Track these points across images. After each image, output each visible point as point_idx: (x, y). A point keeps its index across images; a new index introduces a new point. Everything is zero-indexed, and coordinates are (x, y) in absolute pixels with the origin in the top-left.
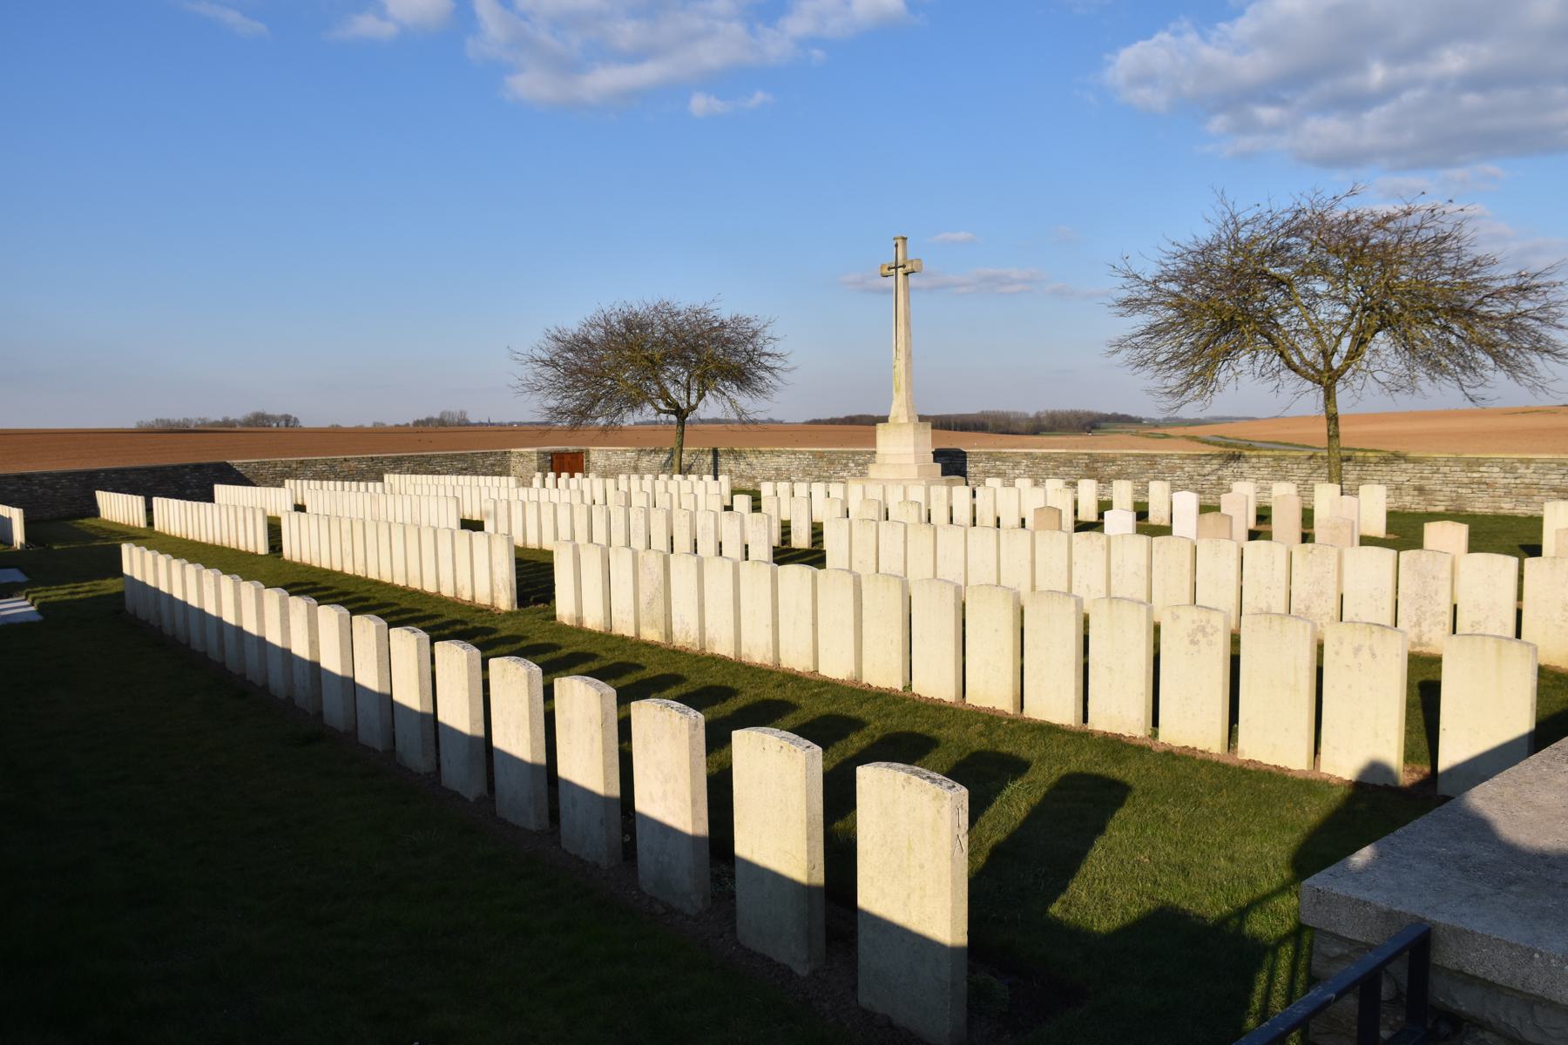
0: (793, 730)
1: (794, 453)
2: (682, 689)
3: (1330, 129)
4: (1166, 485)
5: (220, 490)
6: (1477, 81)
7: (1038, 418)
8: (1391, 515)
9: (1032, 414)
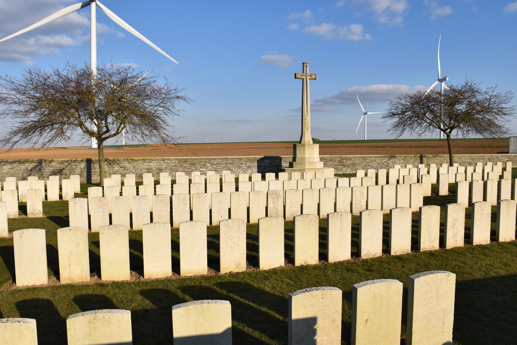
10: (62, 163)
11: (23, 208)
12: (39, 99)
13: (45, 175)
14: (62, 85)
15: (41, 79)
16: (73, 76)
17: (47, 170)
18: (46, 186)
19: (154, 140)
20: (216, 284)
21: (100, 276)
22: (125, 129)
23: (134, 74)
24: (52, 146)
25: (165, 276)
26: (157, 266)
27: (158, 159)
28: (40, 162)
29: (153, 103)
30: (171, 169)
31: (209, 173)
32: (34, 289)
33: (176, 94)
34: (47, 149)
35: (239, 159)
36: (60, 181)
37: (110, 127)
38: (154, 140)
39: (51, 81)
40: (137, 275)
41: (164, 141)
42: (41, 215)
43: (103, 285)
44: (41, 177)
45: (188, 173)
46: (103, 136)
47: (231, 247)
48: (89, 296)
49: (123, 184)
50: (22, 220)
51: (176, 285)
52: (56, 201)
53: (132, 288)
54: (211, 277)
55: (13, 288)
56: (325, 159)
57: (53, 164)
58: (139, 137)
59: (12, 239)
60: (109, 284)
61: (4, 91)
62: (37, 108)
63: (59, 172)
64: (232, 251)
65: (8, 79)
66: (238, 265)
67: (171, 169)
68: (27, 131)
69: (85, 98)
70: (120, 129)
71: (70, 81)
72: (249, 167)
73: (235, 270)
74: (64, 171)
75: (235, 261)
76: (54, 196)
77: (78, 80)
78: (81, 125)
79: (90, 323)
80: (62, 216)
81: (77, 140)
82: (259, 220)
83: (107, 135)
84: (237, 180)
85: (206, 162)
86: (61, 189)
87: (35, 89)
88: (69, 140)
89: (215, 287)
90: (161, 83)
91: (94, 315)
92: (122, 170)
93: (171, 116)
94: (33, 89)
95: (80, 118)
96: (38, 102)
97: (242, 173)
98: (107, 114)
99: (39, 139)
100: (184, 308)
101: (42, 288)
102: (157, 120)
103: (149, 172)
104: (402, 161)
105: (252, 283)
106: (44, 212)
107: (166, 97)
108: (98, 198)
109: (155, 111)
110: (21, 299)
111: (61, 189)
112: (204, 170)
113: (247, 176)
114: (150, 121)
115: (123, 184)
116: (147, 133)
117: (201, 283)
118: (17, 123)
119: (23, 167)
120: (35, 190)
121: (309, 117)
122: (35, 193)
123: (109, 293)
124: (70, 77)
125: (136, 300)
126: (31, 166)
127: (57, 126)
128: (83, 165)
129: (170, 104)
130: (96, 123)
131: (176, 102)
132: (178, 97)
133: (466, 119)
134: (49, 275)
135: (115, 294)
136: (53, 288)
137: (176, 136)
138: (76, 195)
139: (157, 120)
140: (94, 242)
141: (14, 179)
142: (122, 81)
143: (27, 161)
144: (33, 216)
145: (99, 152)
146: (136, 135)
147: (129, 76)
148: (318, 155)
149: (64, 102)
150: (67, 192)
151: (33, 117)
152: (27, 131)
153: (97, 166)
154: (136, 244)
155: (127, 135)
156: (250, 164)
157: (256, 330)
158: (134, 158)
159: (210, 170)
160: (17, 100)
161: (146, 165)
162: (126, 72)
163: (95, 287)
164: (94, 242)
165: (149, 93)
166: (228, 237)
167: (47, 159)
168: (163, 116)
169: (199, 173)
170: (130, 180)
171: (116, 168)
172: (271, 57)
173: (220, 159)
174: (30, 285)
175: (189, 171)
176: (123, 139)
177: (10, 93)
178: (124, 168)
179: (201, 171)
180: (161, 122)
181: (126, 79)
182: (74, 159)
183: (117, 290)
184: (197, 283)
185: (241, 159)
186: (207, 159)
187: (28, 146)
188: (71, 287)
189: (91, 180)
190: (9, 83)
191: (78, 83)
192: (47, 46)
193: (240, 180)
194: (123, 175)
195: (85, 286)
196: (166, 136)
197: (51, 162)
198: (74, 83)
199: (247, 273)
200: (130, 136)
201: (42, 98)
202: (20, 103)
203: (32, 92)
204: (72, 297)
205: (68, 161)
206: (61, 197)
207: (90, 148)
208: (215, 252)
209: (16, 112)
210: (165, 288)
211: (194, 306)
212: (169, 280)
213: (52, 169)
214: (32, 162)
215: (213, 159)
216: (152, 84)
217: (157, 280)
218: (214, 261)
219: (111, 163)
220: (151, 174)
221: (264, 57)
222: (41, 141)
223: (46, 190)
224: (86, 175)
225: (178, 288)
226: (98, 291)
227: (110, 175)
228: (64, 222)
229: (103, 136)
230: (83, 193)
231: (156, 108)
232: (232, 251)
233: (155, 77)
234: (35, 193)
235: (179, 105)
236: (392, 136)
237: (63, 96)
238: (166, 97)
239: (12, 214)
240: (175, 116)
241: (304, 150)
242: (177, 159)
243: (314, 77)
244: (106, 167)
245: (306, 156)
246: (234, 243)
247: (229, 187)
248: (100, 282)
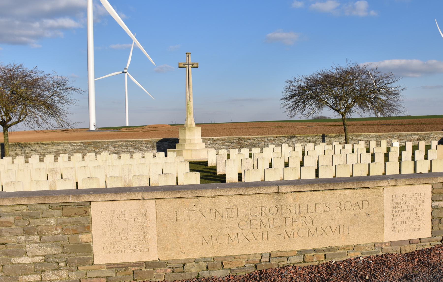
27: (65, 143)
56: (223, 140)
85: (108, 145)
104: (302, 141)
114: (51, 109)
121: (192, 102)
133: (362, 98)
148: (200, 137)
158: (43, 142)
172: (278, 35)
173: (122, 141)
185: (141, 142)
186: (110, 142)
192: (52, 28)
215: (115, 142)
221: (270, 35)
236: (285, 117)
241: (185, 132)
242: (82, 142)
243: (195, 65)
245: (187, 138)
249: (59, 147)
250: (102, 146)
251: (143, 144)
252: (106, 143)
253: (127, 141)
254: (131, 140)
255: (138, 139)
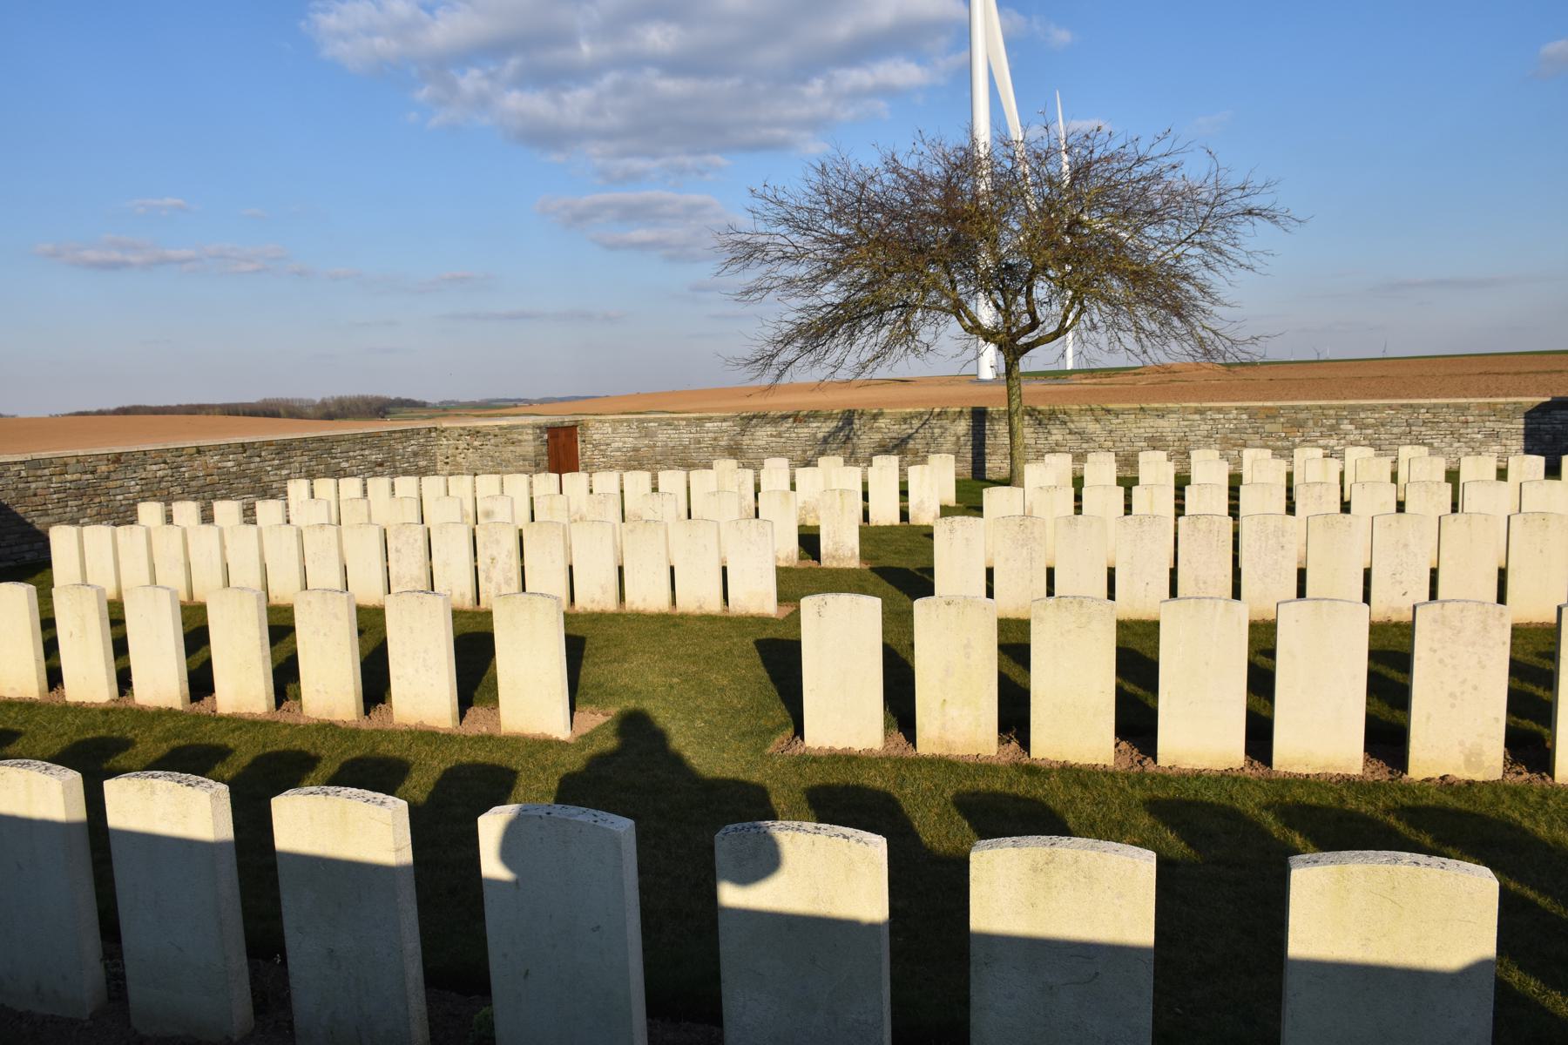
0: (330, 783)
1: (476, 433)
2: (328, 768)
3: (535, 104)
4: (784, 462)
5: (1122, 489)
6: (674, 66)
7: (324, 404)
8: (1528, 451)
9: (318, 400)
10: (905, 420)
11: (809, 541)
12: (847, 242)
13: (861, 453)
14: (907, 200)
15: (852, 186)
16: (935, 171)
17: (866, 439)
18: (865, 485)
19: (1175, 352)
20: (1394, 810)
21: (1025, 744)
22: (1085, 317)
23: (1114, 147)
24: (882, 372)
25: (1222, 766)
26: (1199, 731)
28: (848, 418)
29: (1171, 232)
30: (1225, 440)
31: (1352, 454)
32: (848, 759)
33: (1246, 200)
34: (868, 384)
35: (1457, 407)
36: (903, 473)
37: (1041, 313)
38: (1175, 352)
39: (878, 188)
40: (1135, 752)
41: (1207, 353)
42: (855, 563)
43: (1033, 771)
44: (852, 459)
45: (1285, 453)
46: (1023, 340)
47: (1452, 695)
48: (996, 795)
49: (1078, 482)
50: (807, 571)
51: (1260, 797)
52: (892, 527)
53: (1122, 790)
54: (1376, 785)
55: (797, 750)
57: (882, 423)
58: (1129, 339)
59: (794, 620)
60: (1052, 770)
61: (761, 227)
62: (842, 267)
63: (897, 446)
64: (1453, 706)
65: (769, 193)
66: (1471, 758)
67: (1225, 440)
68: (816, 333)
69: (972, 232)
70: (1071, 316)
71: (926, 183)
72: (1495, 435)
73: (1462, 773)
74: (911, 444)
75: (1461, 743)
76: (885, 513)
77: (949, 179)
78: (958, 309)
79: (1035, 870)
80: (911, 567)
81: (953, 354)
82: (1560, 609)
83: (1034, 335)
84: (1452, 476)
85: (1339, 419)
86: (904, 493)
87: (836, 215)
88: (929, 355)
89: (1392, 820)
90: (1193, 171)
91: (1047, 849)
92: (1073, 442)
93: (1227, 274)
94: (831, 216)
95: (954, 289)
96: (842, 251)
97: (1467, 454)
98: (1033, 273)
99: (848, 356)
100: (1332, 868)
101: (869, 759)
102: (1185, 285)
103: (1154, 448)
105: (1527, 823)
106: (863, 556)
107: (1212, 215)
108: (1017, 520)
109: (1178, 259)
110: (817, 781)
111: (904, 493)
112: (1332, 442)
113: (1489, 464)
114: (1162, 293)
115: (1078, 482)
116: (1154, 327)
117: (1342, 800)
118: (788, 310)
119: (804, 431)
120: (842, 492)
122: (839, 499)
123: (1055, 796)
124: (926, 172)
125: (1136, 827)
126: (823, 428)
127: (893, 314)
128: (963, 426)
129: (1224, 235)
130: (1001, 303)
131: (1245, 227)
132: (1250, 212)
134: (887, 727)
135: (1072, 801)
136: (900, 762)
137: (1243, 335)
138: (945, 511)
139: (1185, 285)
140: (1014, 648)
141: (784, 462)
142: (1077, 172)
143: (814, 415)
144: (835, 565)
145: (1009, 388)
146: (1121, 334)
147: (1096, 156)
149: (917, 244)
150: (922, 502)
151: (831, 293)
152: (816, 333)
153: (1002, 428)
154: (1137, 663)
155: (1093, 335)
156: (1497, 426)
157: (1554, 988)
158: (1110, 406)
159: (1355, 444)
160: (791, 249)
161: (1149, 425)
162: (1089, 143)
163: (1012, 773)
164: (1014, 648)
165: (1158, 202)
166: (1441, 661)
167: (867, 410)
168: (1201, 274)
169: (1320, 452)
170: (1102, 471)
171: (1057, 434)
173: (1390, 407)
174: (839, 747)
175: (1284, 448)
176: (1068, 353)
177: (774, 230)
178: (1081, 434)
179: (1325, 447)
180: (1194, 292)
181: (1089, 165)
182: (937, 410)
183: (1077, 791)
184: (1330, 799)
186: (1344, 408)
187: (818, 374)
188: (946, 765)
189: (983, 469)
190: (771, 206)
191: (950, 190)
192: (857, 94)
193: (1464, 477)
194: (1080, 458)
195: (981, 768)
196: (1212, 336)
197: (875, 417)
198: (937, 191)
199: (1506, 788)
200: (1103, 339)
201: (851, 238)
202: (796, 258)
203: (828, 224)
204: (949, 794)
205: (921, 414)
206: (904, 515)
207: (975, 380)
208: (1386, 708)
209: (790, 282)
210: (1224, 800)
211: (1364, 867)
212: (1235, 779)
213: (877, 437)
214: (829, 417)
215: (1364, 408)
216: (1168, 177)
217: (1198, 775)
218: (1387, 736)
219: (1041, 419)
220: (1162, 455)
222: (851, 360)
223: (865, 497)
224: (969, 456)
225: (1267, 807)
226: (1021, 788)
227: (1040, 456)
228: (919, 582)
229: (1023, 340)
230: (968, 502)
231: (1178, 250)
232: (1453, 706)
233: (1177, 152)
234: (839, 499)
235: (1252, 235)
237: (909, 230)
238: (1212, 215)
239: (782, 555)
240: (1241, 272)
242: (1246, 409)
244: (1027, 433)
246: (1464, 681)
247: (1430, 499)
248: (1025, 760)
249: (1161, 422)
250: (1316, 424)
251: (1471, 419)
252: (1332, 412)
253: (1411, 406)
254: (1427, 401)
255: (1452, 401)
